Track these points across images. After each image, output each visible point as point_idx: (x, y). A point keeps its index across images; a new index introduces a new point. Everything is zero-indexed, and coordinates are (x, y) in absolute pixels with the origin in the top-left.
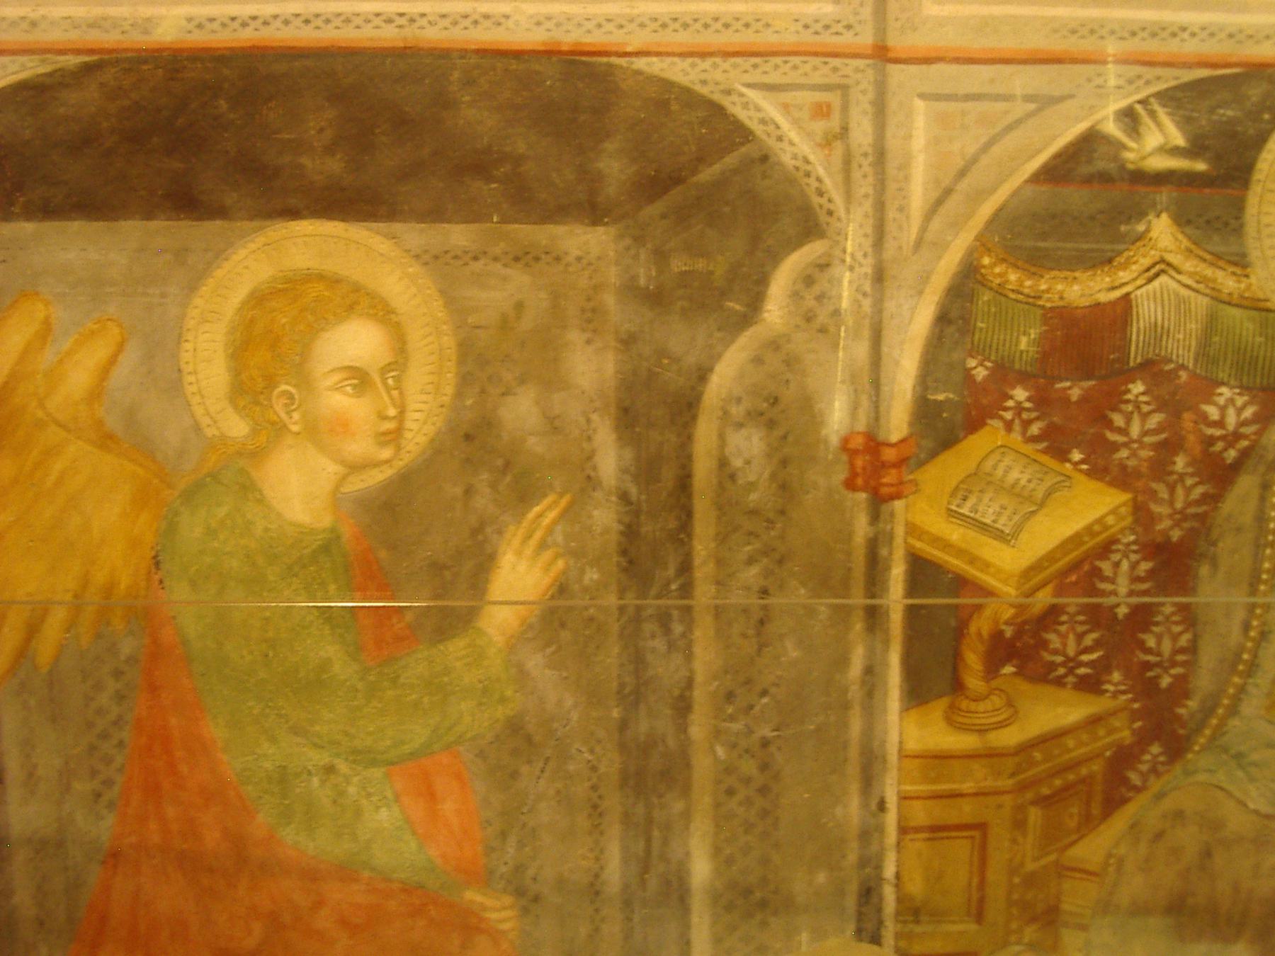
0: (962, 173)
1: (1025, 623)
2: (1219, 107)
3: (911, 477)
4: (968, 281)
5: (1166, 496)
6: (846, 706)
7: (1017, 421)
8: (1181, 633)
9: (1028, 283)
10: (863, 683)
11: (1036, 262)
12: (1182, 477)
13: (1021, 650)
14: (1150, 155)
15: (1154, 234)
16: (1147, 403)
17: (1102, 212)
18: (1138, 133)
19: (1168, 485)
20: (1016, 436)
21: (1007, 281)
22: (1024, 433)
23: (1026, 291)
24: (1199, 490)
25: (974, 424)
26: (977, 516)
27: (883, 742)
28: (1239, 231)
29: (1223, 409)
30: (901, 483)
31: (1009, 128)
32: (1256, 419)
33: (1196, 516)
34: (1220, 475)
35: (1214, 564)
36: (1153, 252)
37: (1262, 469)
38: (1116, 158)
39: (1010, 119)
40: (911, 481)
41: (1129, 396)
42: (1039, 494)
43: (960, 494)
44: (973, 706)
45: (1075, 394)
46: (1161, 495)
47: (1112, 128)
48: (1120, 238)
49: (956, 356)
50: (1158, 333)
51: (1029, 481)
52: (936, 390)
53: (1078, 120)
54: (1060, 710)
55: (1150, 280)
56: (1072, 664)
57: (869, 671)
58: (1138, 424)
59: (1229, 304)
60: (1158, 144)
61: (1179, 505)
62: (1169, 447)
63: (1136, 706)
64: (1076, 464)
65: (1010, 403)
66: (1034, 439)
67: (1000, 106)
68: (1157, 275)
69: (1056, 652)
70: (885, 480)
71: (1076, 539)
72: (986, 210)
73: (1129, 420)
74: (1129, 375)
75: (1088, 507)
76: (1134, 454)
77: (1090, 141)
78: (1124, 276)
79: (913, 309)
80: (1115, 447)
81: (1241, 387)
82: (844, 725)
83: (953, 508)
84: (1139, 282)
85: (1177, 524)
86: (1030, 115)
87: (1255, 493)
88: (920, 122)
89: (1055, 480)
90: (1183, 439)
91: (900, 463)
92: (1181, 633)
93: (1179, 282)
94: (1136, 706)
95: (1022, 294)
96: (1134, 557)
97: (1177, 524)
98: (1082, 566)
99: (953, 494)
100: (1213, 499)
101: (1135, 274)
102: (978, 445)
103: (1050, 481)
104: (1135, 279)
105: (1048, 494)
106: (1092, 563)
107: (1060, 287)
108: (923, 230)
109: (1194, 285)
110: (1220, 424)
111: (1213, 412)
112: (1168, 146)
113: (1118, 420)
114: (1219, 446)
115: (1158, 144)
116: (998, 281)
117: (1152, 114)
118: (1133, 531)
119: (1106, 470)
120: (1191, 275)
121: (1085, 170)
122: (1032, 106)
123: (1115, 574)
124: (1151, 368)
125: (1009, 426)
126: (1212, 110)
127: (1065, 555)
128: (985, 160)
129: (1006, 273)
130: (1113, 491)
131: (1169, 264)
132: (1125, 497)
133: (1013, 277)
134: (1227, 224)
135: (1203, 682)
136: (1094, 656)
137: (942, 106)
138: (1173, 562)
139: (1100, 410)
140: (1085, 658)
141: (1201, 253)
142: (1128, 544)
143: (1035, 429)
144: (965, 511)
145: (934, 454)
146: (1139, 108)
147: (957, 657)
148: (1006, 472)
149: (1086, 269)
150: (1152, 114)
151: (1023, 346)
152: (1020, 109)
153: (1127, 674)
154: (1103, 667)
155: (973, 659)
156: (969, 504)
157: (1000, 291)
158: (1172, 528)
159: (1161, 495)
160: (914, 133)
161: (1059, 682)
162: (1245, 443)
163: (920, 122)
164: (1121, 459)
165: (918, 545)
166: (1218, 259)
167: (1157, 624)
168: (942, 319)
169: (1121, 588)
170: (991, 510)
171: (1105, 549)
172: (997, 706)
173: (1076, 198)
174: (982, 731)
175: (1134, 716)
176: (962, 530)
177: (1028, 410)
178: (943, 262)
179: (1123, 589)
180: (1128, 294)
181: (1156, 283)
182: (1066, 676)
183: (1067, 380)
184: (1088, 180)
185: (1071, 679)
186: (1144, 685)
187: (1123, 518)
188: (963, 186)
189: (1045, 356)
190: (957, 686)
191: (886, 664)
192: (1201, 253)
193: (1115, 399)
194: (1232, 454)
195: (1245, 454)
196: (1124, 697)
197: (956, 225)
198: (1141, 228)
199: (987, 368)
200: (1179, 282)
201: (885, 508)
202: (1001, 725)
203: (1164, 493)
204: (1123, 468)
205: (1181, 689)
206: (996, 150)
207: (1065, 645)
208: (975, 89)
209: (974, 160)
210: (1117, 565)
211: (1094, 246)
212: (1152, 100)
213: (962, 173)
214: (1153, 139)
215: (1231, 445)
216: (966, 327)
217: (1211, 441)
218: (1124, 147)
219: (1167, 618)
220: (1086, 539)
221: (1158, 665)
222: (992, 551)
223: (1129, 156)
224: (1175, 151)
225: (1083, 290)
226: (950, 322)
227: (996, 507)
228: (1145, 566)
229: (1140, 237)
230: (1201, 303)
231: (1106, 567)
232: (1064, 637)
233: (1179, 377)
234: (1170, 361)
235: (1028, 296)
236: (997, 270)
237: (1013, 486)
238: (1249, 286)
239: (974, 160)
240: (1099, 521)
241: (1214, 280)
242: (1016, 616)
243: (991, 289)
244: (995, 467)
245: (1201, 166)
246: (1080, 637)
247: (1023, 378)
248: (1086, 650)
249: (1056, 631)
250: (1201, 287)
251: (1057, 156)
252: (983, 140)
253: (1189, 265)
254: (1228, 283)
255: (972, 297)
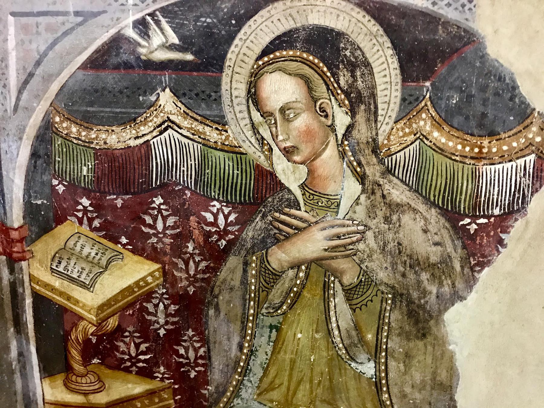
0: (38, 63)
1: (104, 335)
2: (202, 16)
3: (28, 248)
4: (46, 134)
5: (184, 267)
6: (13, 372)
7: (85, 218)
8: (200, 348)
9: (84, 134)
10: (19, 361)
11: (87, 120)
12: (192, 255)
13: (103, 350)
14: (156, 50)
15: (162, 102)
16: (165, 210)
17: (127, 88)
18: (149, 36)
19: (183, 260)
20: (85, 228)
21: (71, 132)
22: (90, 225)
23: (83, 138)
24: (203, 264)
25: (60, 220)
26: (69, 273)
27: (35, 394)
28: (218, 100)
29: (216, 216)
30: (24, 251)
31: (66, 34)
32: (237, 222)
33: (203, 280)
34: (216, 256)
35: (217, 309)
36: (162, 114)
37: (243, 253)
38: (134, 52)
39: (68, 26)
40: (28, 250)
41: (154, 205)
42: (104, 262)
43: (57, 260)
44: (79, 379)
45: (119, 203)
46: (180, 266)
47: (131, 33)
48: (140, 105)
49: (45, 178)
50: (168, 167)
51: (97, 254)
52: (36, 198)
53: (108, 27)
54: (130, 386)
55: (161, 133)
56: (134, 360)
57: (21, 354)
58: (161, 223)
59: (216, 149)
60: (160, 44)
61: (192, 273)
62: (182, 237)
63: (176, 387)
64: (124, 246)
65: (80, 207)
66: (96, 230)
67: (60, 19)
68: (166, 129)
69: (123, 353)
70: (15, 249)
71: (129, 289)
72: (55, 87)
73: (155, 220)
74: (153, 192)
75: (132, 272)
76: (160, 240)
77: (117, 41)
78: (144, 130)
79: (18, 148)
80: (148, 236)
81: (227, 202)
82: (12, 382)
83: (54, 267)
84: (155, 134)
85: (191, 284)
86: (80, 24)
87: (241, 267)
88: (12, 30)
89: (113, 254)
90: (191, 232)
91: (21, 240)
92: (200, 348)
93: (181, 134)
94: (176, 387)
95: (80, 140)
96: (166, 302)
97: (191, 284)
98: (134, 305)
99: (53, 259)
100: (214, 270)
101: (152, 128)
102: (66, 230)
103: (109, 254)
104: (152, 132)
105: (109, 263)
106: (141, 304)
107: (104, 136)
108: (18, 99)
109: (191, 136)
110: (215, 224)
111: (210, 217)
112: (167, 45)
113: (149, 220)
114: (215, 237)
115: (160, 44)
116: (65, 132)
117: (158, 23)
118: (164, 287)
119: (143, 249)
120: (189, 130)
121: (114, 60)
122: (80, 19)
123: (156, 311)
124: (165, 189)
125: (81, 222)
126: (197, 19)
127: (82, 308)
128: (51, 54)
129: (71, 127)
130: (150, 262)
131: (173, 122)
132: (157, 266)
133: (74, 129)
134: (210, 96)
135: (216, 375)
136: (148, 357)
137: (24, 20)
138: (192, 307)
139: (136, 213)
140: (142, 357)
141: (195, 116)
142: (163, 294)
143: (96, 223)
144: (61, 269)
145: (39, 236)
146: (149, 18)
147: (66, 350)
148: (82, 248)
149: (119, 125)
150: (158, 23)
151: (85, 172)
152: (74, 20)
153: (168, 367)
154: (152, 364)
155: (75, 353)
156: (64, 264)
157: (66, 138)
158: (189, 286)
159: (180, 266)
160: (9, 37)
161: (127, 370)
162: (231, 237)
163: (12, 30)
164: (153, 243)
165: (38, 287)
166: (205, 120)
167: (185, 341)
168: (34, 155)
169: (160, 317)
170: (76, 270)
171: (149, 296)
172: (93, 381)
173: (110, 78)
174: (86, 394)
175: (175, 392)
176: (61, 281)
177: (91, 212)
178: (32, 120)
179: (162, 321)
180: (148, 141)
181: (166, 134)
182: (131, 366)
183: (114, 194)
184: (117, 67)
185: (134, 368)
186: (178, 374)
187: (158, 279)
188: (39, 71)
189: (98, 180)
190: (68, 369)
191: (28, 350)
192: (195, 116)
193: (146, 207)
194: (223, 243)
195: (230, 243)
196: (167, 381)
197: (38, 97)
198: (153, 98)
199: (64, 185)
200: (181, 134)
201: (16, 265)
202: (95, 392)
203: (182, 265)
204: (154, 249)
205: (203, 379)
206: (57, 47)
207: (129, 349)
208: (44, 9)
209: (45, 54)
210: (156, 306)
211: (123, 110)
212: (157, 13)
213: (38, 63)
214: (157, 39)
215: (221, 238)
216: (49, 159)
217: (209, 235)
218: (139, 45)
219: (191, 338)
220: (136, 290)
221: (188, 364)
222: (77, 293)
223: (142, 51)
224: (172, 47)
225: (119, 138)
226: (39, 157)
227: (78, 268)
228: (173, 308)
229: (153, 105)
230: (195, 148)
231: (150, 307)
232: (128, 345)
233: (186, 194)
234: (179, 184)
235: (84, 142)
236: (65, 125)
237: (87, 257)
238: (227, 137)
239: (45, 54)
240: (143, 279)
241: (205, 133)
242: (97, 331)
243: (62, 137)
244: (75, 245)
245: (189, 57)
246: (137, 346)
247: (87, 193)
248: (143, 353)
249: (122, 341)
250: (196, 137)
251: (97, 51)
252: (50, 42)
253: (186, 123)
254: (213, 135)
255: (51, 142)
